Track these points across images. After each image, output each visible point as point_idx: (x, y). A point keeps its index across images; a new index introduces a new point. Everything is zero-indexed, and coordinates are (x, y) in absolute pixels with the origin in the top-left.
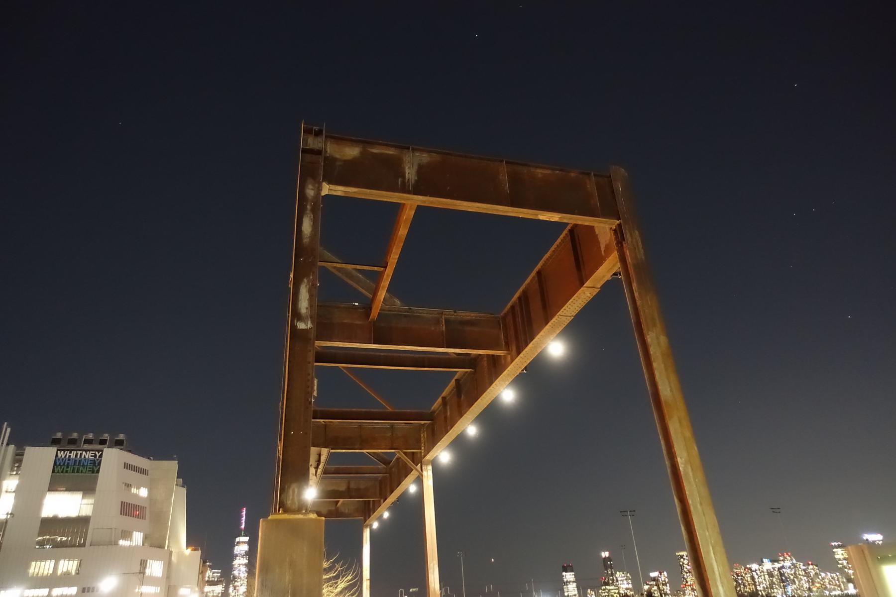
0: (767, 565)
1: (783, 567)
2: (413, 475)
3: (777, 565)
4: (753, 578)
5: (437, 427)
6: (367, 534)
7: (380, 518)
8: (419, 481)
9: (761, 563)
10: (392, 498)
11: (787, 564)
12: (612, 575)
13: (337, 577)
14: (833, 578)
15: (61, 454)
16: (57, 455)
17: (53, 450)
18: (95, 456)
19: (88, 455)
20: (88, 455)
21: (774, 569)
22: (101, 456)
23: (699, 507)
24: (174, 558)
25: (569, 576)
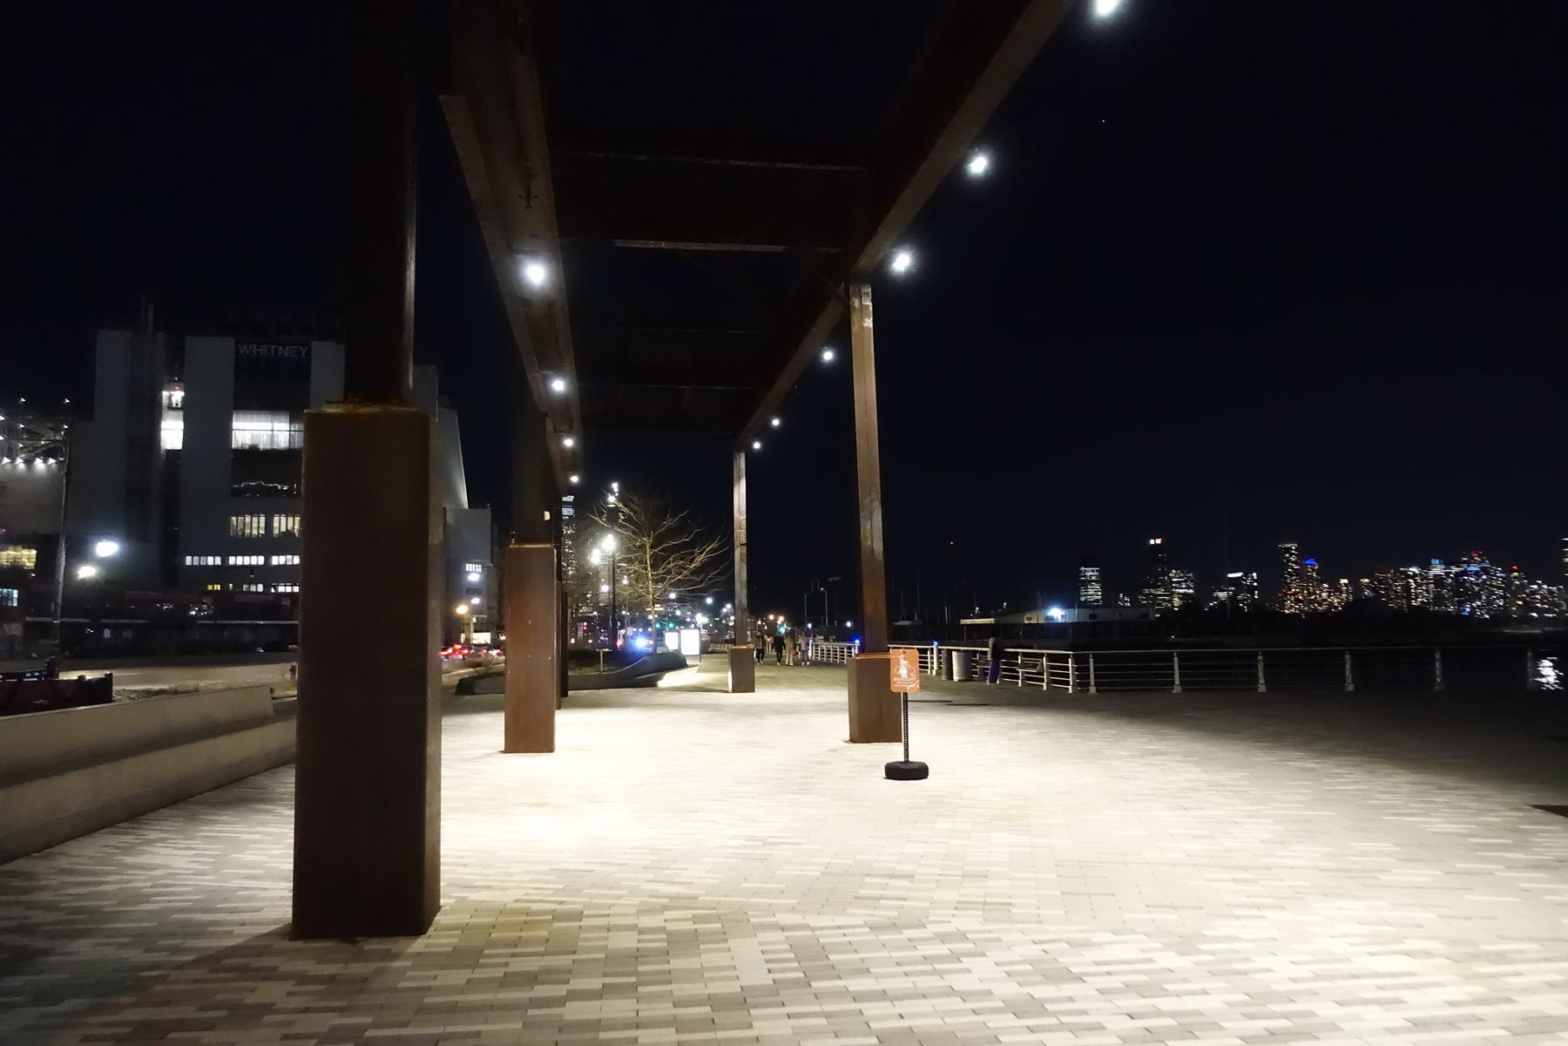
0: (1437, 570)
1: (1465, 573)
2: (825, 323)
3: (1455, 569)
4: (1407, 588)
5: (880, 168)
6: (741, 462)
7: (765, 433)
8: (842, 337)
9: (1426, 565)
10: (785, 383)
11: (1474, 568)
12: (1166, 574)
13: (691, 545)
14: (1550, 592)
15: (244, 349)
16: (237, 352)
17: (230, 342)
18: (300, 353)
19: (287, 352)
20: (287, 352)
21: (1447, 574)
22: (308, 354)
23: (65, 1006)
24: (450, 518)
25: (1091, 573)
